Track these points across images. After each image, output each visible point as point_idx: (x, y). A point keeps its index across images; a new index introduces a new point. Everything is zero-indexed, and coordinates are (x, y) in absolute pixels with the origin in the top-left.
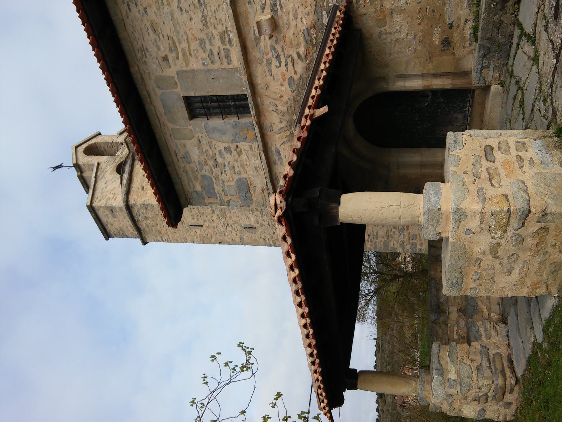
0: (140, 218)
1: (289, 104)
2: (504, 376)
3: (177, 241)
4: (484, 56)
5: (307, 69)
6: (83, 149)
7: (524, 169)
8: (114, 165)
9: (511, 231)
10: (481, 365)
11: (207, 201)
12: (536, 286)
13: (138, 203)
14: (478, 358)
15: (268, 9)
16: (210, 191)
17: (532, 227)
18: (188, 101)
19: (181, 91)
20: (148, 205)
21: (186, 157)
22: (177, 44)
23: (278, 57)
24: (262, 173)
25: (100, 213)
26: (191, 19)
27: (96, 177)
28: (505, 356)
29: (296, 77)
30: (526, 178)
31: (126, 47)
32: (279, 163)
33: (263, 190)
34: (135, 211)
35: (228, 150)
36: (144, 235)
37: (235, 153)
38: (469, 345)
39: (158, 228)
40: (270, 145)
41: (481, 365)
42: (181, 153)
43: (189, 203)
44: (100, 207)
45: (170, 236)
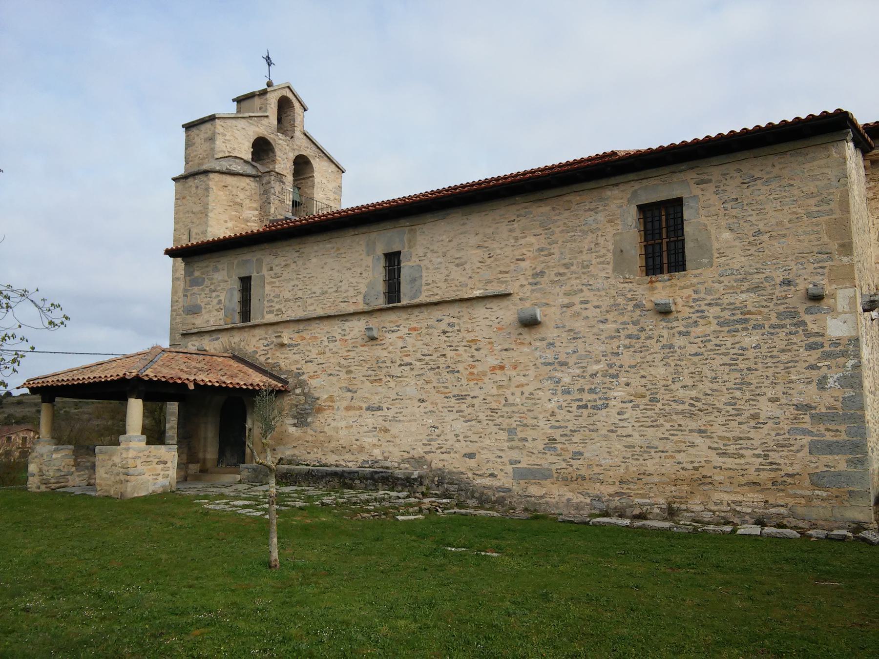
0: (196, 181)
1: (244, 350)
2: (56, 483)
3: (176, 213)
4: (254, 469)
5: (261, 364)
6: (285, 95)
7: (152, 476)
8: (265, 133)
9: (121, 470)
10: (61, 471)
11: (188, 278)
12: (101, 485)
13: (210, 183)
14: (66, 470)
15: (290, 342)
16: (195, 282)
17: (122, 477)
18: (249, 278)
19: (254, 275)
20: (208, 192)
21: (216, 270)
22: (278, 279)
23: (268, 345)
24: (205, 325)
25: (208, 125)
26: (290, 292)
27: (250, 117)
28: (67, 484)
29: (257, 356)
30: (146, 476)
31: (279, 244)
32: (210, 339)
33: (194, 324)
34: (203, 177)
35: (220, 302)
36: (182, 181)
37: (218, 307)
38: (73, 466)
39: (188, 198)
40: (222, 333)
41: (61, 471)
42: (220, 266)
43: (187, 264)
44: (215, 128)
45: (181, 208)
